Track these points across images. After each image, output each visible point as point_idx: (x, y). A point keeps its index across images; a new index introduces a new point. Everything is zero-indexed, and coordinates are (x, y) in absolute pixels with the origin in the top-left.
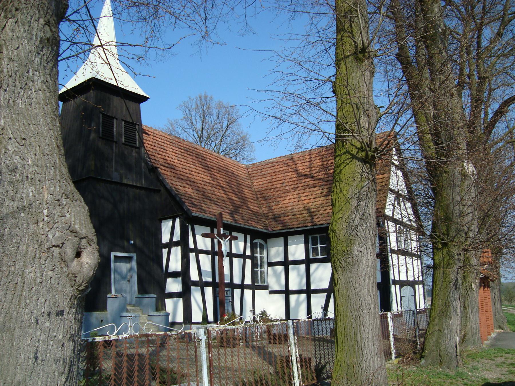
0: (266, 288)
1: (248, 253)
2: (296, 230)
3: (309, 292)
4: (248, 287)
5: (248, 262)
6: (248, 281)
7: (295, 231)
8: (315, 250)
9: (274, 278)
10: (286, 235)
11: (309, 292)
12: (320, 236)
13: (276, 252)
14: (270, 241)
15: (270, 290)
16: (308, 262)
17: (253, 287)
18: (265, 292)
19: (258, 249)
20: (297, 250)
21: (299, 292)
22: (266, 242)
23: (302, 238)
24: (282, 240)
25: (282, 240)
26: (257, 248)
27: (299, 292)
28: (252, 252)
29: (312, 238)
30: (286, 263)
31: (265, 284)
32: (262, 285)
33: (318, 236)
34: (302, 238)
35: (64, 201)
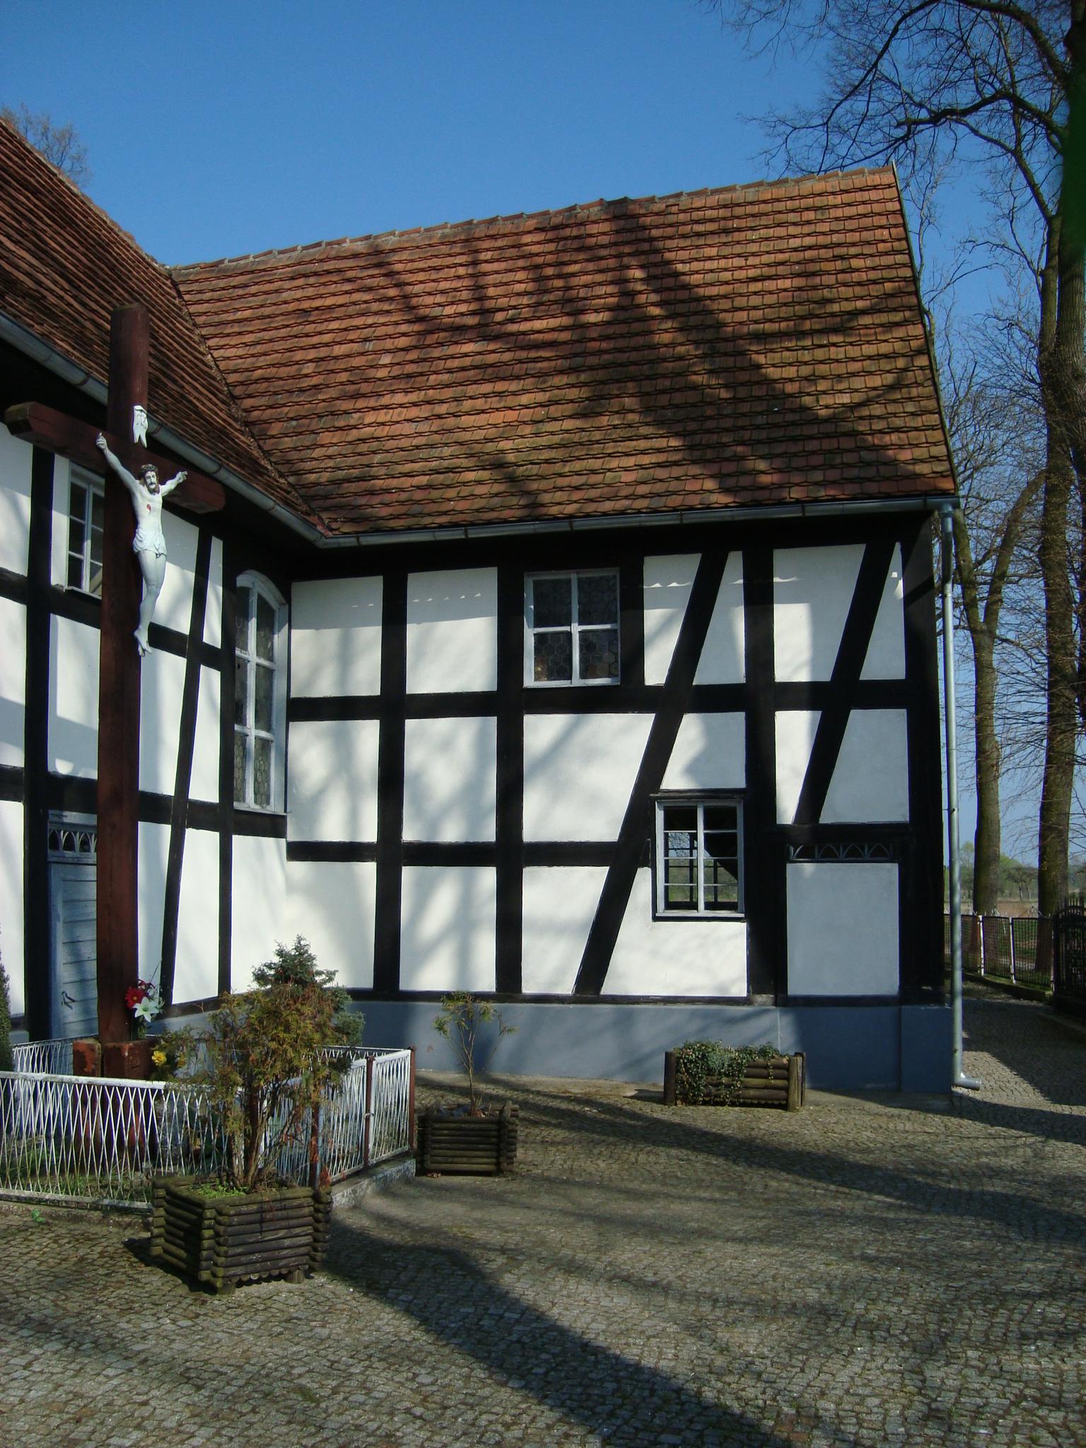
0: (271, 826)
1: (213, 634)
2: (474, 534)
3: (510, 855)
4: (202, 816)
5: (211, 680)
6: (205, 788)
7: (467, 542)
8: (554, 655)
9: (328, 775)
10: (395, 566)
11: (510, 855)
12: (580, 580)
13: (327, 650)
14: (307, 593)
15: (293, 835)
16: (505, 705)
17: (227, 819)
18: (272, 847)
19: (253, 624)
20: (456, 646)
21: (464, 855)
22: (287, 597)
23: (485, 583)
24: (370, 591)
25: (370, 591)
26: (247, 618)
27: (464, 855)
28: (231, 632)
29: (537, 585)
30: (394, 707)
31: (275, 807)
32: (256, 808)
33: (574, 577)
34: (485, 583)
35: (63, 837)
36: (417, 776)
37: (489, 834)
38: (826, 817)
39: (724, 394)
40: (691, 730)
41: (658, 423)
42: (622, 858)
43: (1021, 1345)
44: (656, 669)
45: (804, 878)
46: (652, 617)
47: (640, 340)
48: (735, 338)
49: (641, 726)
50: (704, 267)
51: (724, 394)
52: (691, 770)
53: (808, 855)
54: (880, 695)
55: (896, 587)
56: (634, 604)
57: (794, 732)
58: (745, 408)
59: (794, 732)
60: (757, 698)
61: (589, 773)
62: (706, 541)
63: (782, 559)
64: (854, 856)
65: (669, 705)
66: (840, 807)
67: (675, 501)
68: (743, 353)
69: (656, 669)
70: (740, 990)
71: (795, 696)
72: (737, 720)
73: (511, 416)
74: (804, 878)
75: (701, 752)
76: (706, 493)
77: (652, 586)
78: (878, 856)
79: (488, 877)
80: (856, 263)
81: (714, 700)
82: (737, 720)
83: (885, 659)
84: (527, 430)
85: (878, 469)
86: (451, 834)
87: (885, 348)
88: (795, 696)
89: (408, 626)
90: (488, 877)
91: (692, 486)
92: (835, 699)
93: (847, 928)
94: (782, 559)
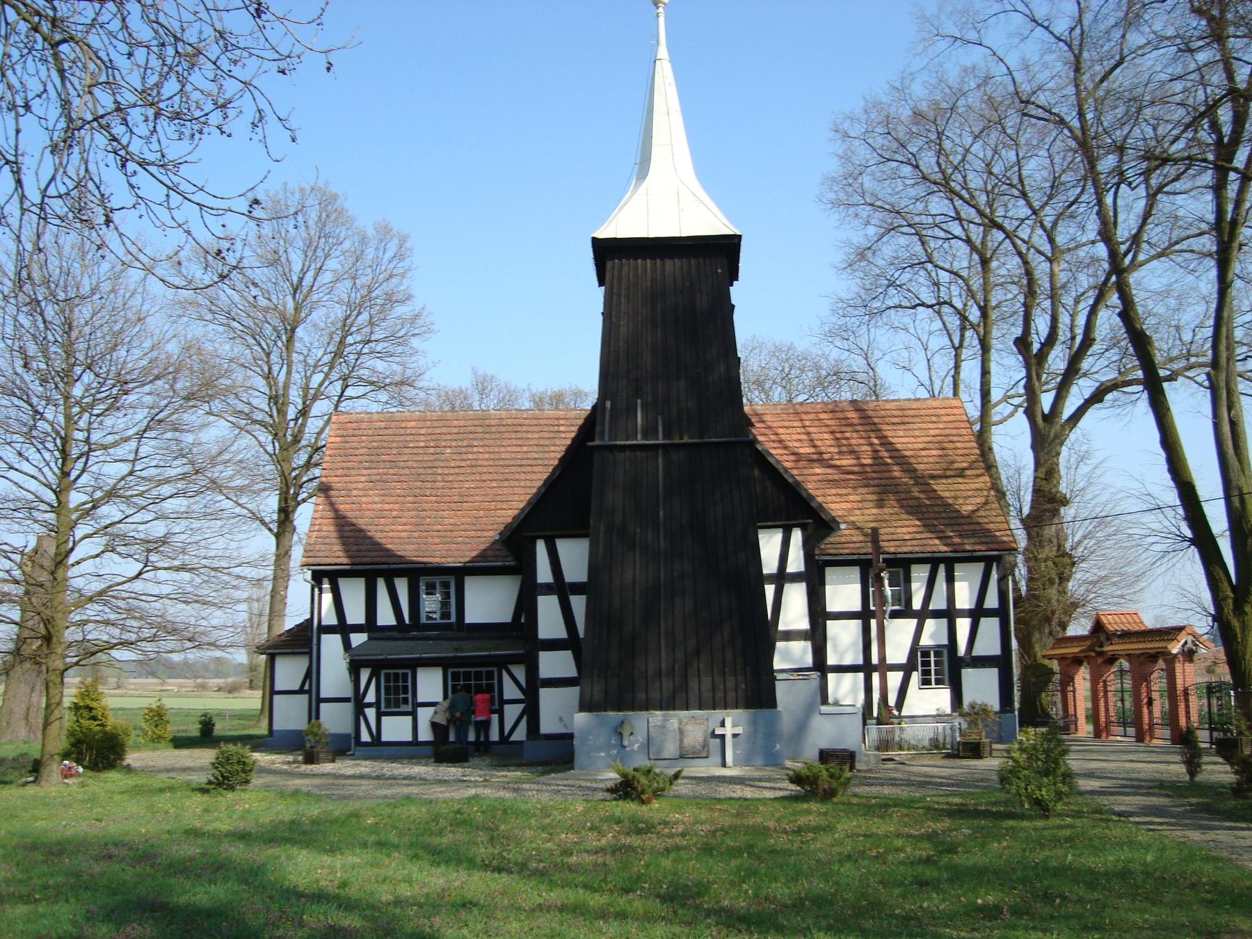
16: (864, 615)
21: (852, 669)
27: (852, 669)
34: (855, 572)
36: (834, 639)
37: (860, 661)
38: (974, 653)
39: (928, 502)
40: (930, 624)
41: (909, 513)
42: (908, 668)
43: (834, 895)
44: (917, 604)
45: (968, 674)
46: (914, 586)
47: (887, 475)
48: (923, 477)
49: (912, 624)
50: (902, 440)
51: (928, 502)
52: (932, 636)
53: (968, 666)
54: (990, 613)
55: (994, 576)
56: (908, 580)
57: (963, 625)
58: (936, 509)
59: (963, 625)
60: (949, 614)
61: (899, 638)
62: (933, 562)
63: (957, 566)
64: (983, 666)
65: (923, 615)
66: (978, 651)
67: (929, 549)
68: (929, 484)
69: (917, 604)
70: (948, 711)
71: (963, 613)
72: (945, 621)
73: (849, 506)
74: (968, 674)
75: (933, 633)
76: (937, 546)
77: (914, 575)
78: (991, 666)
79: (861, 675)
80: (959, 445)
81: (937, 614)
82: (945, 621)
83: (992, 601)
84: (858, 512)
85: (984, 534)
86: (848, 661)
87: (978, 486)
88: (963, 613)
89: (828, 588)
90: (861, 675)
91: (931, 542)
92: (977, 613)
93: (982, 687)
94: (957, 566)
